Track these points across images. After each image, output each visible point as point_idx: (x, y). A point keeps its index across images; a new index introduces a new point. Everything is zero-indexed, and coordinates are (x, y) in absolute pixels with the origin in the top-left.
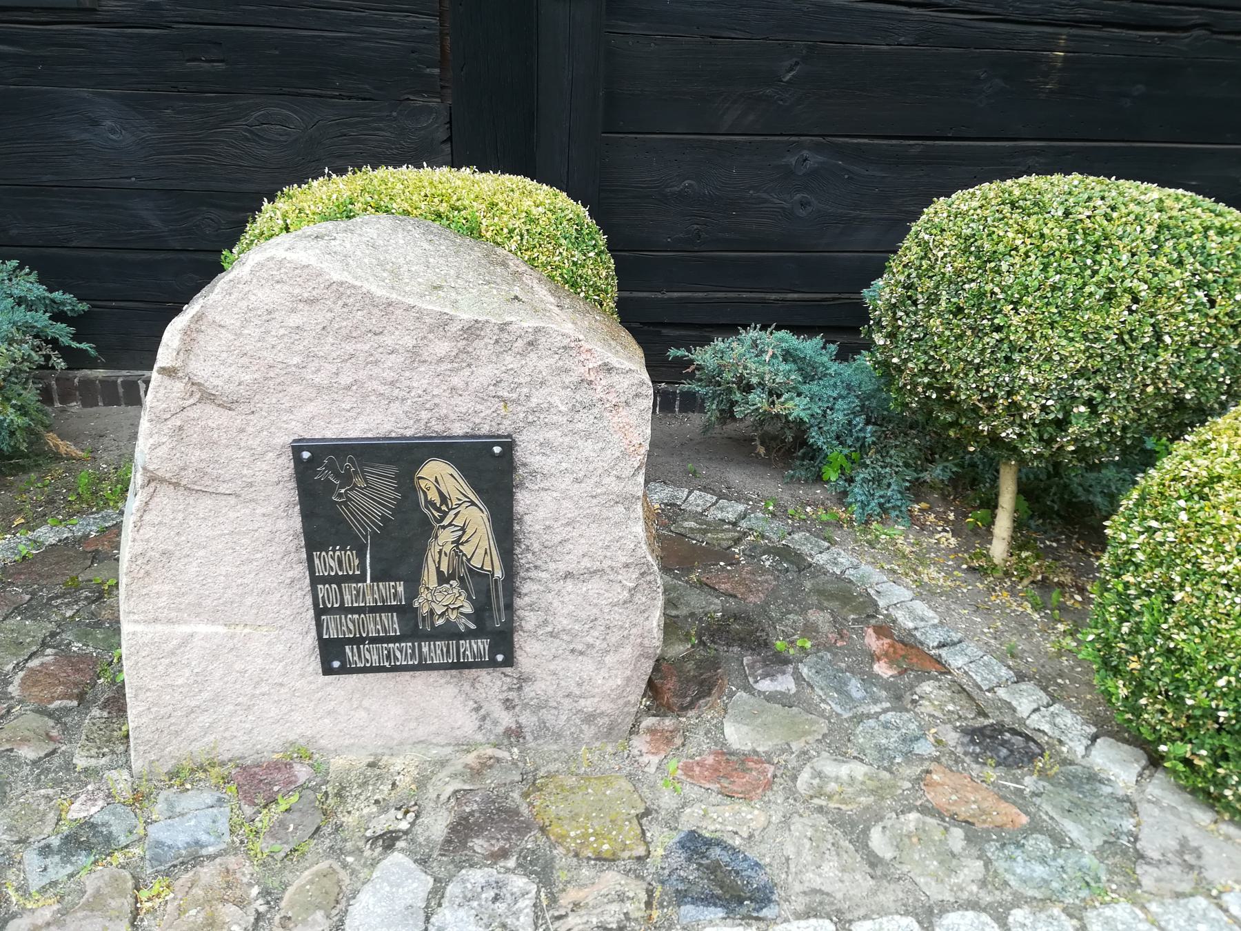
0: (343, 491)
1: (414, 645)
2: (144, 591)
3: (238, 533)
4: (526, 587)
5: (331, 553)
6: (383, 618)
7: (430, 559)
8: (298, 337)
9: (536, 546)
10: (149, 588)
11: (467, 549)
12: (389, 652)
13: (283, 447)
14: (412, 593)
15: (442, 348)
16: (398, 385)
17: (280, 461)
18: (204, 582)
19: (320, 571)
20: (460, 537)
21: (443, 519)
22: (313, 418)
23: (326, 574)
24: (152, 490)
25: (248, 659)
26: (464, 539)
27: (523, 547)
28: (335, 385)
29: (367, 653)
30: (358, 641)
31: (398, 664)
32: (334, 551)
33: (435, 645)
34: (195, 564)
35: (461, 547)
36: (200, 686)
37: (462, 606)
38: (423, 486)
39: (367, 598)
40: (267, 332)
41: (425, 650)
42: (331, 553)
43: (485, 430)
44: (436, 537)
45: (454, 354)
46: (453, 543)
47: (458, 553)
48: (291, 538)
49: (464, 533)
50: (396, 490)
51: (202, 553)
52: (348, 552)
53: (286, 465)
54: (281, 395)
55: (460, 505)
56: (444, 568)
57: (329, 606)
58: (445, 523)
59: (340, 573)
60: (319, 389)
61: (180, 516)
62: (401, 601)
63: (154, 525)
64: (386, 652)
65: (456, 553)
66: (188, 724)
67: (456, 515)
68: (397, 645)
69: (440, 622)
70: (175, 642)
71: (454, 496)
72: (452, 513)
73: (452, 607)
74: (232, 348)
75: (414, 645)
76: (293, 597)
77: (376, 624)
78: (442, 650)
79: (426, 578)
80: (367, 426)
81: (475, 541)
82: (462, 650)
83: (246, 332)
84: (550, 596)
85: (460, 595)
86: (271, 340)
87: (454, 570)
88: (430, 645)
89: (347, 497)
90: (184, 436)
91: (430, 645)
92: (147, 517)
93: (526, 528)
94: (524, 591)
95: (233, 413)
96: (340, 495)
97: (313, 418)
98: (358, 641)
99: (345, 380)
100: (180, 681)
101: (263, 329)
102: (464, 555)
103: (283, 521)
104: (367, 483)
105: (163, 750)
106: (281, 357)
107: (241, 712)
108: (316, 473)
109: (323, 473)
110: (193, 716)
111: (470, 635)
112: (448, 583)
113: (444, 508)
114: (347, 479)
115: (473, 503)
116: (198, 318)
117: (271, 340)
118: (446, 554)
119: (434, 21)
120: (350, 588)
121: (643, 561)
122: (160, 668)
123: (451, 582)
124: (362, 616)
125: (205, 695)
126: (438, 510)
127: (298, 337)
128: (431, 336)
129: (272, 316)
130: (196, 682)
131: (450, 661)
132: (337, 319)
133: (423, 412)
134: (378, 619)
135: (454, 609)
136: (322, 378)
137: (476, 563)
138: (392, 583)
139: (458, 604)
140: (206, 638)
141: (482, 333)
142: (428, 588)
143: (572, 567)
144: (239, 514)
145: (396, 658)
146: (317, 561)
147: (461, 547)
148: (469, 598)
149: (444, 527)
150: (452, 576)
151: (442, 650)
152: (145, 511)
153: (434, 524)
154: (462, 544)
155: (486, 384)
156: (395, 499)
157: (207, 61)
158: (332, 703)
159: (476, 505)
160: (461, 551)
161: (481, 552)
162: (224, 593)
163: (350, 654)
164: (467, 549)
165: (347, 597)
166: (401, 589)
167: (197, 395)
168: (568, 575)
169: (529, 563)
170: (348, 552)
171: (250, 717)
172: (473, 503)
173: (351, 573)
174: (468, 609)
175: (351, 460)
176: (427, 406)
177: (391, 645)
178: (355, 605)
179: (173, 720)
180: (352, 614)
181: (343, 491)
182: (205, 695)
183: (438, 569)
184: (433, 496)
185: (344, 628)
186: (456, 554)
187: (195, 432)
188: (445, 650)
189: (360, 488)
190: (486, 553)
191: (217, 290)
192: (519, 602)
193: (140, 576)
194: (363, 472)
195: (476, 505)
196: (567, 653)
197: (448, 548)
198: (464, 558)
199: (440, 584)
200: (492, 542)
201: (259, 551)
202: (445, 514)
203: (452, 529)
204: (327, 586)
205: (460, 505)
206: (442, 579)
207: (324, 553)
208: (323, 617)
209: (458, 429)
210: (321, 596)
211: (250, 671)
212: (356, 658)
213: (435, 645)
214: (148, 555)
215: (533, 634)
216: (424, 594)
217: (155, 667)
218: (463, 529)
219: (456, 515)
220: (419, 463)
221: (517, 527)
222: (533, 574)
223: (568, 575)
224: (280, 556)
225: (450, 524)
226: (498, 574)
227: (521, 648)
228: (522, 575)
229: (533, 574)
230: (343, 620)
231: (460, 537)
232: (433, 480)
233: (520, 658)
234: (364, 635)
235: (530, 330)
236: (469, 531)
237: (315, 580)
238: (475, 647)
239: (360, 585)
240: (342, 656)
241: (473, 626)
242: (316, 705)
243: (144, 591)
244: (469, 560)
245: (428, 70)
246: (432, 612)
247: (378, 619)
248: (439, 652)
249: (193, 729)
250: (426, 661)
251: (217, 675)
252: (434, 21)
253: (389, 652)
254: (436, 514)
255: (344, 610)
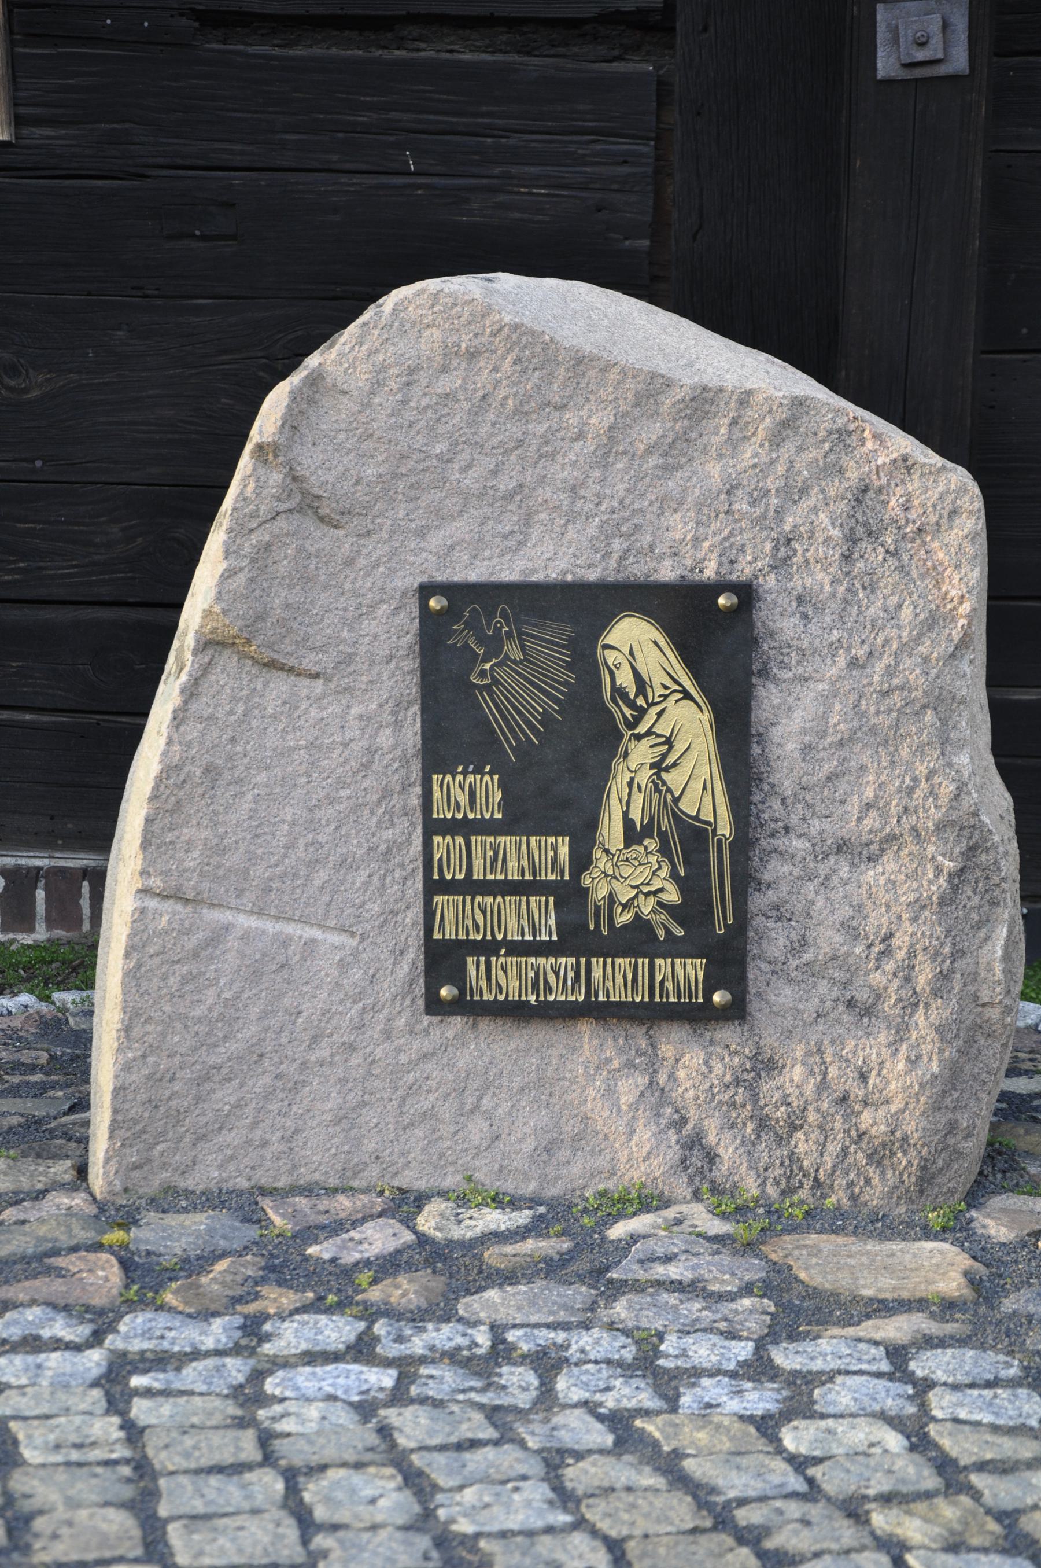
0: (487, 666)
1: (578, 963)
2: (169, 837)
3: (319, 748)
4: (776, 870)
5: (460, 777)
6: (533, 906)
7: (614, 796)
8: (446, 410)
9: (788, 787)
10: (176, 833)
11: (674, 779)
12: (537, 974)
13: (404, 594)
14: (581, 861)
15: (652, 431)
16: (582, 492)
17: (397, 620)
18: (259, 831)
19: (441, 812)
20: (664, 756)
21: (637, 720)
22: (452, 548)
23: (449, 816)
24: (207, 660)
25: (305, 989)
26: (670, 760)
27: (766, 787)
28: (491, 492)
29: (501, 973)
30: (488, 948)
31: (551, 998)
32: (465, 773)
33: (613, 963)
34: (249, 797)
35: (664, 775)
36: (227, 1029)
37: (661, 890)
38: (610, 662)
39: (510, 865)
40: (405, 402)
41: (597, 973)
42: (460, 777)
43: (710, 572)
44: (626, 755)
45: (670, 440)
46: (653, 766)
47: (658, 786)
48: (396, 765)
49: (671, 747)
50: (569, 666)
51: (262, 778)
52: (487, 778)
53: (409, 621)
54: (412, 505)
55: (666, 697)
56: (636, 815)
57: (449, 877)
58: (642, 729)
59: (471, 816)
60: (466, 497)
61: (240, 709)
62: (562, 876)
63: (200, 719)
64: (531, 974)
65: (656, 785)
66: (198, 1099)
67: (660, 714)
68: (552, 960)
69: (623, 918)
70: (201, 935)
71: (658, 679)
72: (654, 711)
73: (646, 889)
74: (354, 425)
75: (578, 963)
76: (389, 879)
77: (519, 916)
78: (625, 976)
79: (605, 833)
80: (530, 565)
81: (687, 766)
82: (658, 978)
83: (377, 400)
84: (811, 887)
85: (660, 868)
86: (409, 415)
87: (651, 819)
88: (605, 964)
89: (493, 677)
90: (270, 562)
91: (605, 964)
92: (193, 707)
93: (774, 752)
94: (767, 877)
95: (341, 532)
96: (483, 674)
97: (452, 548)
98: (488, 948)
99: (506, 483)
100: (199, 1011)
101: (399, 397)
102: (669, 790)
103: (388, 731)
104: (524, 653)
105: (151, 1148)
106: (419, 442)
107: (281, 1095)
108: (450, 634)
109: (460, 636)
110: (207, 1086)
111: (673, 949)
112: (640, 843)
113: (641, 702)
114: (494, 646)
115: (687, 695)
116: (315, 380)
117: (409, 415)
118: (640, 790)
119: (645, 149)
120: (483, 844)
121: (972, 822)
122: (172, 981)
123: (646, 842)
124: (499, 899)
125: (233, 1047)
126: (632, 705)
127: (446, 410)
128: (637, 412)
129: (416, 377)
130: (221, 1017)
131: (638, 999)
132: (505, 382)
133: (617, 541)
134: (524, 907)
135: (647, 895)
136: (470, 481)
137: (688, 806)
138: (551, 840)
139: (657, 884)
140: (246, 937)
141: (713, 409)
142: (607, 851)
143: (849, 829)
144: (325, 714)
145: (548, 989)
146: (437, 793)
147: (664, 775)
148: (674, 875)
149: (639, 737)
150: (647, 830)
151: (625, 976)
152: (192, 695)
153: (622, 728)
154: (667, 770)
155: (714, 490)
156: (566, 684)
157: (203, 238)
158: (431, 1097)
159: (692, 699)
160: (664, 783)
161: (697, 785)
162: (285, 856)
163: (474, 974)
164: (674, 779)
165: (478, 864)
166: (564, 851)
167: (297, 498)
168: (842, 847)
169: (776, 820)
170: (487, 778)
171: (295, 1108)
172: (687, 695)
173: (487, 816)
174: (672, 896)
175: (504, 615)
176: (624, 529)
177: (542, 961)
178: (490, 877)
179: (177, 1086)
180: (483, 895)
181: (487, 666)
182: (233, 1047)
183: (626, 814)
184: (625, 679)
185: (469, 923)
186: (657, 790)
187: (286, 557)
188: (630, 977)
189: (514, 662)
190: (705, 788)
191: (342, 340)
192: (758, 902)
193: (169, 807)
194: (520, 634)
195: (692, 699)
196: (841, 1008)
197: (645, 776)
198: (669, 797)
199: (627, 846)
200: (715, 769)
201: (345, 785)
202: (641, 713)
203: (652, 740)
204: (448, 838)
205: (666, 697)
206: (632, 835)
207: (449, 778)
208: (436, 899)
209: (667, 573)
210: (437, 857)
211: (305, 1014)
212: (483, 983)
213: (613, 963)
214: (186, 769)
215: (779, 970)
216: (602, 862)
217: (164, 978)
218: (669, 742)
219: (660, 714)
220: (605, 621)
221: (756, 750)
222: (780, 842)
223: (842, 847)
224: (375, 797)
225: (649, 733)
226: (725, 829)
227: (759, 995)
228: (764, 843)
229: (780, 842)
230: (468, 907)
231: (664, 756)
232: (626, 651)
233: (758, 1015)
234: (500, 937)
235: (785, 402)
236: (679, 747)
237: (433, 827)
238: (680, 972)
239: (499, 839)
240: (459, 978)
241: (679, 932)
242: (404, 1100)
243: (169, 837)
244: (676, 800)
245: (627, 243)
246: (611, 899)
247: (524, 907)
248: (619, 979)
249: (203, 1113)
250: (597, 996)
251: (255, 1011)
252: (645, 149)
253: (537, 974)
254: (628, 712)
255: (470, 887)
